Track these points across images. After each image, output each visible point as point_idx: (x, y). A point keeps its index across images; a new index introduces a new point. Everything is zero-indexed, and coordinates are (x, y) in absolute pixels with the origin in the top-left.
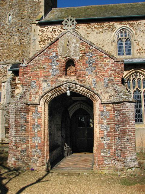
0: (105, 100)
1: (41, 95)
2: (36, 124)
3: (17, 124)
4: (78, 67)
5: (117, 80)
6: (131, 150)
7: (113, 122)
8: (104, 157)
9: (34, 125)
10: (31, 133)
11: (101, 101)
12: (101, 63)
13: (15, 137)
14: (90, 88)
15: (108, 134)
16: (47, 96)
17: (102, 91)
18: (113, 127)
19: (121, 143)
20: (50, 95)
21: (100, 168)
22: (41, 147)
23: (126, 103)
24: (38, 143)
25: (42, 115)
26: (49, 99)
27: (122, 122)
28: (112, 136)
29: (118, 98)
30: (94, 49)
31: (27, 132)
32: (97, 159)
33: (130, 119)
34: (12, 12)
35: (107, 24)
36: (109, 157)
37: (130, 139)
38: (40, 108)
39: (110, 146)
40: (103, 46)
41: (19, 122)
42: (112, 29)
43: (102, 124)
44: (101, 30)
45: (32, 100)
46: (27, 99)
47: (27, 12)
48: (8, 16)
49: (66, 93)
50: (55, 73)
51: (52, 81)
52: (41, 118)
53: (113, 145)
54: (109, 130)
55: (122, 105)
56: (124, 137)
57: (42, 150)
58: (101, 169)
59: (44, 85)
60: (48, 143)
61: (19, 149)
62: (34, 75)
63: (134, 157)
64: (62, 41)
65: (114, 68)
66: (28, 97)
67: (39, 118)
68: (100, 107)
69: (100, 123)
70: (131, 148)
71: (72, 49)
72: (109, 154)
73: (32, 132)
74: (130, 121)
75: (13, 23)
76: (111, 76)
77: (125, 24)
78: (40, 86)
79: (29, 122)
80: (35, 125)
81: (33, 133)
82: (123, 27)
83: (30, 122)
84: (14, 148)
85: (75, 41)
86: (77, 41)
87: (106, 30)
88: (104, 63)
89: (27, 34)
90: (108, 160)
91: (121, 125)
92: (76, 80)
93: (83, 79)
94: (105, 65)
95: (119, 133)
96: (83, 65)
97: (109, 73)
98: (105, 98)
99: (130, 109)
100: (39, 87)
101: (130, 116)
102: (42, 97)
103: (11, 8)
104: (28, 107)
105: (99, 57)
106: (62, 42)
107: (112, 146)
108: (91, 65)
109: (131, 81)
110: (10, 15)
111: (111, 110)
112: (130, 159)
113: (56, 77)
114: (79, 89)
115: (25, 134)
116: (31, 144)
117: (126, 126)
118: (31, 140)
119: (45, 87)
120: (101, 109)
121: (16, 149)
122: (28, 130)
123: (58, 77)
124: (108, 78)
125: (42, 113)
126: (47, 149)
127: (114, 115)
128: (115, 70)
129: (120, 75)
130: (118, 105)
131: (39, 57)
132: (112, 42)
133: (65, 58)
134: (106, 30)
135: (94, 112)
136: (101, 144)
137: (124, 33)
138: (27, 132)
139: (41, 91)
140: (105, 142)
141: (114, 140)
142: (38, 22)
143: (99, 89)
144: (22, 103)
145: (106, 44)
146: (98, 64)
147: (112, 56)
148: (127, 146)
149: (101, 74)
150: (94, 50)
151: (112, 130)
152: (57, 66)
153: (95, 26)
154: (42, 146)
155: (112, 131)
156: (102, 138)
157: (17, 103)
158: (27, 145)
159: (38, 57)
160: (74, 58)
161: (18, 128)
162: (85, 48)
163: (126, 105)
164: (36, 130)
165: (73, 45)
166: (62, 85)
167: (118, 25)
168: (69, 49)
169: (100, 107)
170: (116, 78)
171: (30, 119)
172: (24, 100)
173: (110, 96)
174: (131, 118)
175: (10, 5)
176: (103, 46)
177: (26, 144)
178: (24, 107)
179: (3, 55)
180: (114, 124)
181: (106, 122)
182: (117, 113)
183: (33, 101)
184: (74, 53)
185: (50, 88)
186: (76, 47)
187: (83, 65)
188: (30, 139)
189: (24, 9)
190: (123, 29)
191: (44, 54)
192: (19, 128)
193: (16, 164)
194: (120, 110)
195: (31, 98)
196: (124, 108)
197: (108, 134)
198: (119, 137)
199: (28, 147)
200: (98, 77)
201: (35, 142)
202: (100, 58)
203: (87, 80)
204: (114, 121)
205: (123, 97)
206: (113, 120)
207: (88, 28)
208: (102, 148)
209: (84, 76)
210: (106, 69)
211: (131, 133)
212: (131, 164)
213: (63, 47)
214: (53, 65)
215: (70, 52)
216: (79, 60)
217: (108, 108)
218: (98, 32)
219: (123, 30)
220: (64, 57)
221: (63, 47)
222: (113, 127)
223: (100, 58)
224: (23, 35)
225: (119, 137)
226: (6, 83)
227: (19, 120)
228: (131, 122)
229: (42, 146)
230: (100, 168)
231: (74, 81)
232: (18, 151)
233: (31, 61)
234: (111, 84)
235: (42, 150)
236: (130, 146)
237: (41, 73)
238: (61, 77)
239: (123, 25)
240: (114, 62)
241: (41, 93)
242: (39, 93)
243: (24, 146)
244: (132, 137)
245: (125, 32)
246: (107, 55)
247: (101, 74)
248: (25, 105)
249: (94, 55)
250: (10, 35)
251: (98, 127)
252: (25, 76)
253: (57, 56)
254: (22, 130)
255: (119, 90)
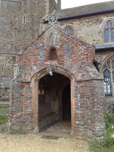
0: (79, 78)
1: (32, 75)
2: (29, 97)
3: (13, 97)
4: (58, 54)
5: (89, 62)
6: (100, 120)
7: (85, 96)
8: (79, 124)
9: (27, 97)
10: (25, 104)
11: (76, 79)
12: (76, 50)
13: (12, 107)
14: (67, 69)
15: (81, 106)
16: (36, 76)
17: (76, 71)
18: (85, 100)
19: (91, 114)
20: (39, 75)
21: (76, 134)
22: (32, 114)
23: (94, 81)
24: (30, 112)
25: (33, 90)
26: (39, 78)
27: (91, 96)
28: (85, 107)
29: (88, 76)
30: (71, 38)
31: (22, 103)
32: (73, 126)
33: (99, 94)
34: (26, 15)
35: (95, 18)
36: (83, 125)
37: (99, 111)
38: (31, 85)
39: (83, 116)
40: (92, 36)
41: (15, 96)
42: (100, 21)
43: (77, 97)
44: (90, 23)
45: (26, 79)
46: (23, 79)
47: (36, 14)
48: (23, 18)
49: (49, 74)
50: (42, 59)
51: (40, 65)
52: (32, 92)
53: (86, 115)
54: (83, 102)
55: (91, 82)
56: (93, 109)
57: (32, 117)
58: (76, 135)
59: (35, 68)
60: (37, 111)
61: (15, 116)
62: (28, 61)
63: (103, 127)
64: (47, 34)
65: (86, 53)
66: (23, 77)
67: (31, 92)
68: (75, 84)
69: (75, 97)
70: (99, 119)
71: (54, 40)
72: (82, 123)
73: (26, 103)
74: (99, 96)
75: (26, 23)
76: (84, 59)
77: (110, 17)
78: (32, 69)
79: (23, 96)
80: (28, 98)
81: (26, 104)
82: (109, 19)
83: (25, 95)
84: (11, 115)
85: (56, 33)
86: (58, 33)
87: (94, 23)
88: (78, 50)
89: (37, 31)
90: (82, 128)
91: (90, 99)
92: (57, 63)
93: (62, 62)
94: (79, 51)
95: (89, 105)
96: (62, 52)
97: (82, 57)
98: (78, 77)
99: (98, 86)
100: (31, 70)
101: (98, 91)
102: (33, 76)
103: (25, 12)
104: (24, 84)
105: (75, 45)
106: (47, 34)
107: (85, 116)
108: (68, 51)
109: (111, 62)
110: (25, 18)
111: (84, 86)
112: (99, 128)
113: (42, 62)
114: (60, 71)
115: (20, 105)
116: (24, 112)
117: (95, 100)
118: (25, 109)
119: (35, 69)
120: (76, 85)
121: (12, 116)
122: (23, 101)
123: (44, 62)
124: (82, 61)
125: (33, 89)
126: (36, 116)
127: (86, 90)
128: (87, 55)
129: (91, 58)
130: (88, 83)
131: (31, 46)
132: (99, 32)
133: (49, 48)
134: (94, 23)
135: (71, 88)
136: (76, 114)
137: (109, 24)
138: (22, 103)
139: (32, 72)
140: (79, 112)
141: (86, 111)
142: (44, 21)
143: (74, 71)
144: (18, 82)
145: (94, 34)
146: (73, 50)
147: (85, 43)
148: (96, 117)
149: (76, 58)
150: (70, 39)
151: (85, 102)
152: (43, 54)
153: (86, 21)
154: (33, 114)
155: (84, 103)
156: (77, 108)
157: (14, 81)
158: (22, 113)
159: (30, 47)
160: (56, 46)
161: (14, 100)
162: (64, 38)
163: (94, 82)
164: (29, 101)
165: (55, 36)
166: (47, 67)
167: (105, 19)
168: (52, 40)
169: (75, 84)
170: (87, 61)
171: (24, 93)
172: (20, 79)
173: (83, 75)
174: (99, 93)
175: (25, 10)
176: (92, 36)
177: (21, 112)
178: (19, 84)
179: (21, 47)
180: (86, 97)
181: (79, 95)
182: (88, 89)
183: (27, 80)
184: (55, 43)
185: (39, 70)
186: (57, 38)
187: (62, 52)
188: (24, 109)
189: (34, 12)
190: (109, 20)
191: (34, 45)
192: (15, 100)
193: (11, 128)
194: (90, 86)
195: (25, 78)
196: (92, 85)
197: (81, 106)
198: (89, 108)
199: (22, 114)
200: (74, 61)
201: (28, 110)
202: (75, 45)
203: (65, 63)
204: (86, 95)
205: (92, 76)
206: (85, 94)
207: (80, 23)
208: (77, 117)
209: (63, 60)
210: (80, 53)
211: (100, 106)
212: (99, 133)
213: (47, 38)
214: (41, 52)
215: (53, 42)
216: (59, 48)
217: (81, 85)
218: (88, 25)
219: (109, 22)
220: (48, 46)
221: (47, 38)
222: (85, 100)
223: (75, 45)
224: (34, 31)
225: (90, 109)
226: (16, 67)
227: (15, 94)
228: (99, 97)
229: (33, 114)
230: (76, 134)
231: (55, 64)
232: (14, 118)
233: (25, 50)
234: (84, 66)
235: (32, 117)
236: (99, 117)
237: (33, 59)
238: (46, 61)
239: (109, 17)
240: (86, 48)
241: (32, 73)
242: (31, 74)
243: (19, 114)
244: (100, 109)
245: (111, 23)
246: (81, 42)
247: (76, 58)
248: (20, 83)
249: (70, 43)
250: (25, 32)
251: (74, 99)
252: (21, 62)
253: (43, 46)
254: (17, 101)
255: (89, 70)
